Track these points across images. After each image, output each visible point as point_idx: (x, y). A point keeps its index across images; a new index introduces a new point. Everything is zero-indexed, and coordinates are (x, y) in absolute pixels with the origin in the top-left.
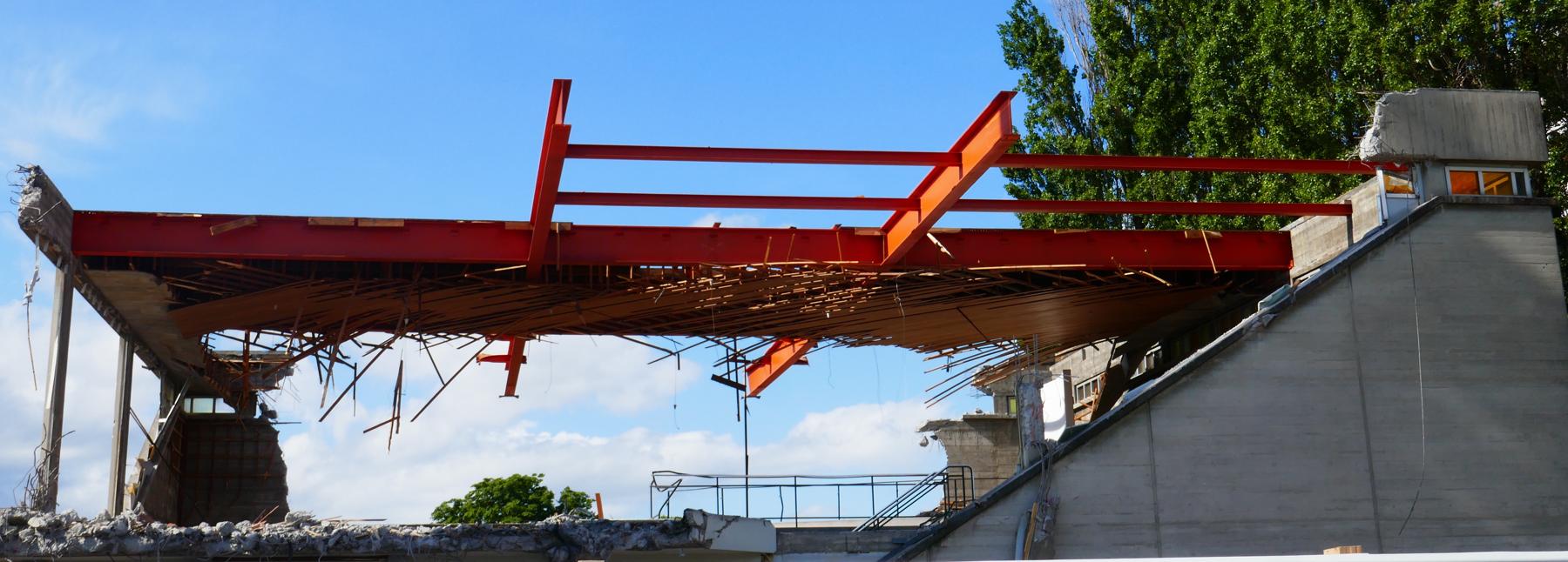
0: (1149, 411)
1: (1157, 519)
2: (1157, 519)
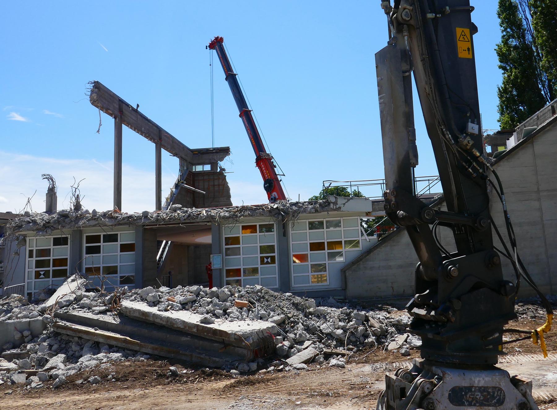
0: (532, 143)
1: (538, 189)
2: (538, 189)
